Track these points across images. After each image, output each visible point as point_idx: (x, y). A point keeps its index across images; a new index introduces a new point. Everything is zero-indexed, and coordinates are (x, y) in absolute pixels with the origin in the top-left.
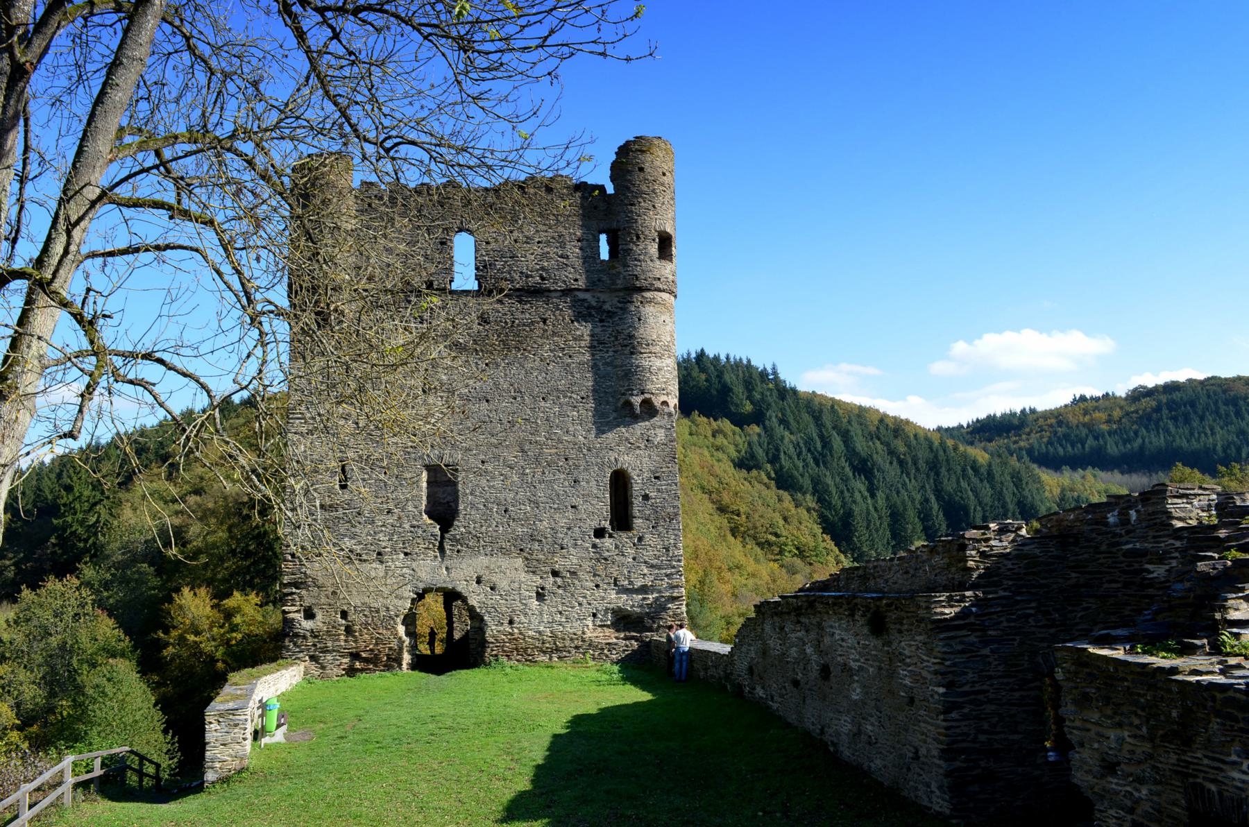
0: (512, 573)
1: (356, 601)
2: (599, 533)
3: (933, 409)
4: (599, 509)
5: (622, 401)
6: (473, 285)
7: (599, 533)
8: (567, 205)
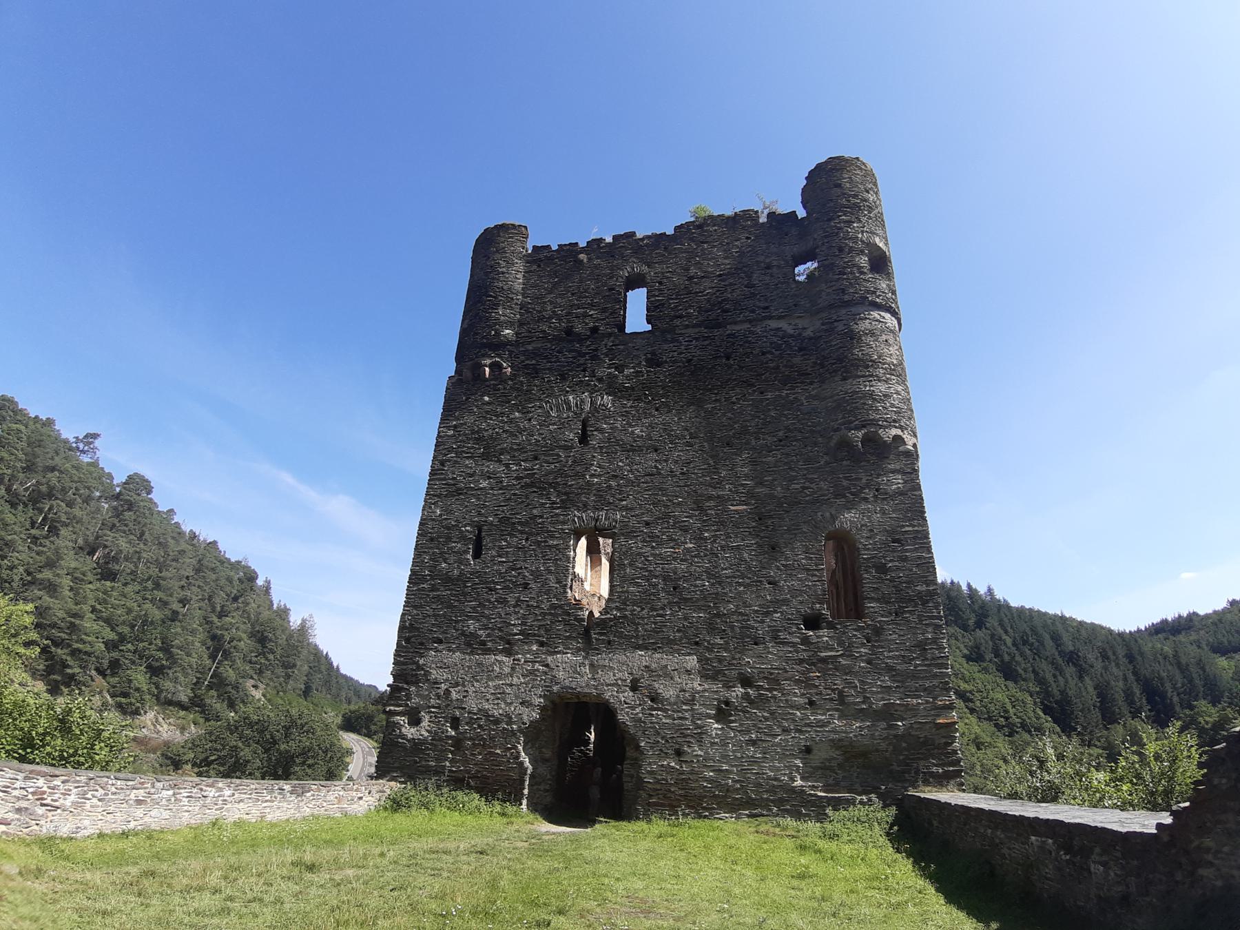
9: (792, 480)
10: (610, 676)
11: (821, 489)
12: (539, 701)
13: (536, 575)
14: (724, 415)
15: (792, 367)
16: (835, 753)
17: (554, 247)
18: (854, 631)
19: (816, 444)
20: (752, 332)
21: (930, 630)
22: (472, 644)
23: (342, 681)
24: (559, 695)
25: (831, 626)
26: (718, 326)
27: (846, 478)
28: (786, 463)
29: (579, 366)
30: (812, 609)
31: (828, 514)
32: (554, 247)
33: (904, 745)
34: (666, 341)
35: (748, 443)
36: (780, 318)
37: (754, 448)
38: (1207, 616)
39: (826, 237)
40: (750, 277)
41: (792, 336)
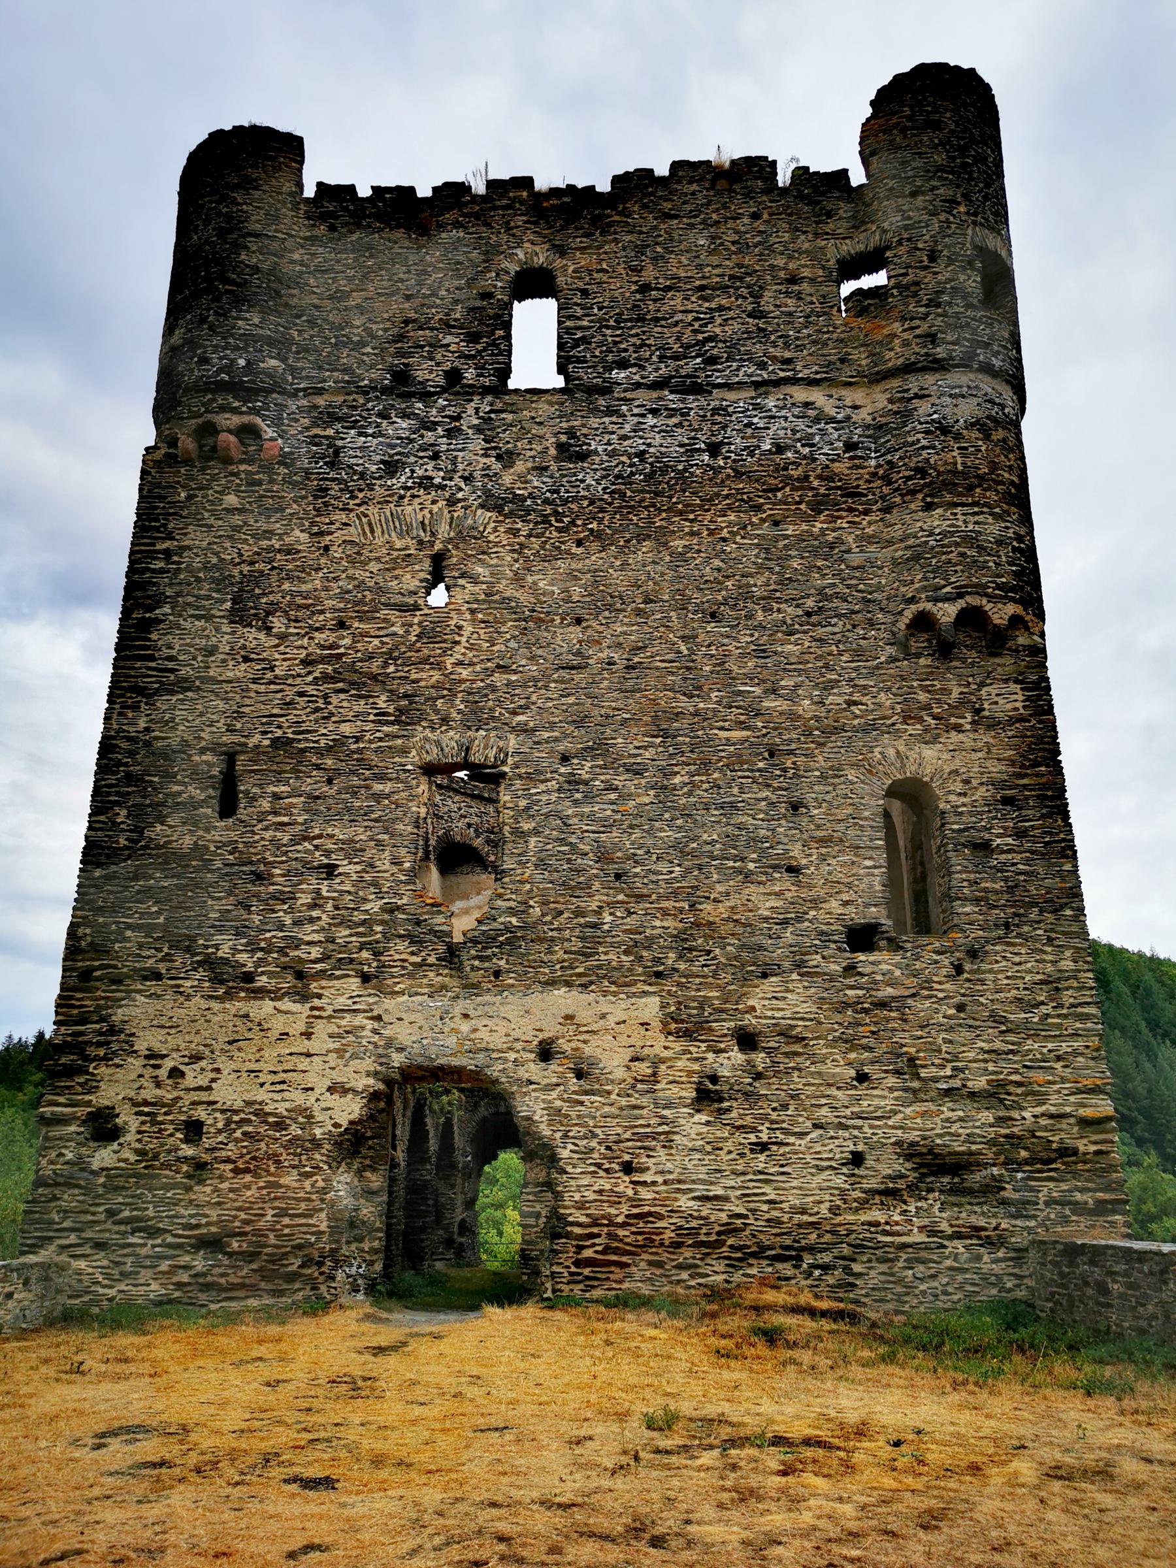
9: (829, 687)
11: (880, 705)
12: (364, 1082)
13: (352, 850)
15: (830, 479)
16: (900, 1166)
17: (364, 192)
18: (933, 959)
19: (871, 624)
21: (1068, 953)
25: (895, 946)
27: (926, 689)
31: (891, 752)
32: (364, 192)
33: (1024, 1154)
34: (595, 411)
35: (750, 616)
36: (812, 383)
39: (906, 228)
40: (757, 297)
41: (832, 420)
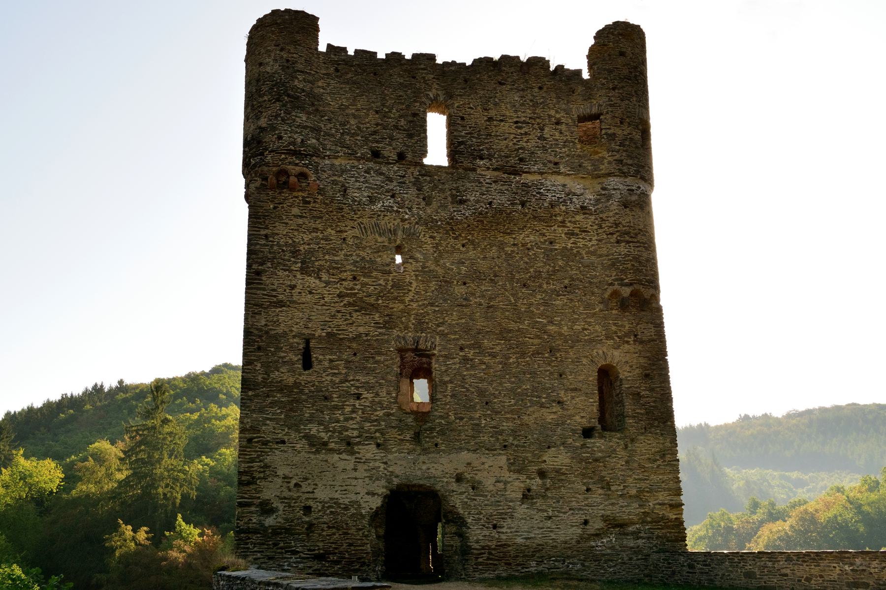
0: (492, 469)
1: (322, 494)
2: (588, 433)
3: (239, 411)
4: (584, 408)
5: (609, 292)
6: (444, 162)
7: (588, 433)
8: (294, 229)
10: (437, 468)
11: (596, 331)
14: (521, 258)
20: (542, 184)
22: (318, 445)
23: (422, 135)
24: (399, 486)
26: (516, 173)
27: (615, 324)
28: (570, 308)
29: (387, 191)
30: (590, 422)
31: (601, 352)
32: (351, 52)
35: (540, 286)
37: (545, 291)
38: (718, 428)
40: (542, 129)
